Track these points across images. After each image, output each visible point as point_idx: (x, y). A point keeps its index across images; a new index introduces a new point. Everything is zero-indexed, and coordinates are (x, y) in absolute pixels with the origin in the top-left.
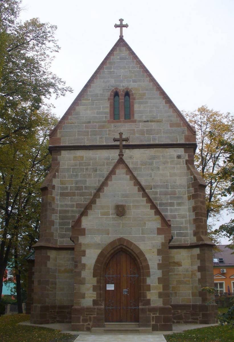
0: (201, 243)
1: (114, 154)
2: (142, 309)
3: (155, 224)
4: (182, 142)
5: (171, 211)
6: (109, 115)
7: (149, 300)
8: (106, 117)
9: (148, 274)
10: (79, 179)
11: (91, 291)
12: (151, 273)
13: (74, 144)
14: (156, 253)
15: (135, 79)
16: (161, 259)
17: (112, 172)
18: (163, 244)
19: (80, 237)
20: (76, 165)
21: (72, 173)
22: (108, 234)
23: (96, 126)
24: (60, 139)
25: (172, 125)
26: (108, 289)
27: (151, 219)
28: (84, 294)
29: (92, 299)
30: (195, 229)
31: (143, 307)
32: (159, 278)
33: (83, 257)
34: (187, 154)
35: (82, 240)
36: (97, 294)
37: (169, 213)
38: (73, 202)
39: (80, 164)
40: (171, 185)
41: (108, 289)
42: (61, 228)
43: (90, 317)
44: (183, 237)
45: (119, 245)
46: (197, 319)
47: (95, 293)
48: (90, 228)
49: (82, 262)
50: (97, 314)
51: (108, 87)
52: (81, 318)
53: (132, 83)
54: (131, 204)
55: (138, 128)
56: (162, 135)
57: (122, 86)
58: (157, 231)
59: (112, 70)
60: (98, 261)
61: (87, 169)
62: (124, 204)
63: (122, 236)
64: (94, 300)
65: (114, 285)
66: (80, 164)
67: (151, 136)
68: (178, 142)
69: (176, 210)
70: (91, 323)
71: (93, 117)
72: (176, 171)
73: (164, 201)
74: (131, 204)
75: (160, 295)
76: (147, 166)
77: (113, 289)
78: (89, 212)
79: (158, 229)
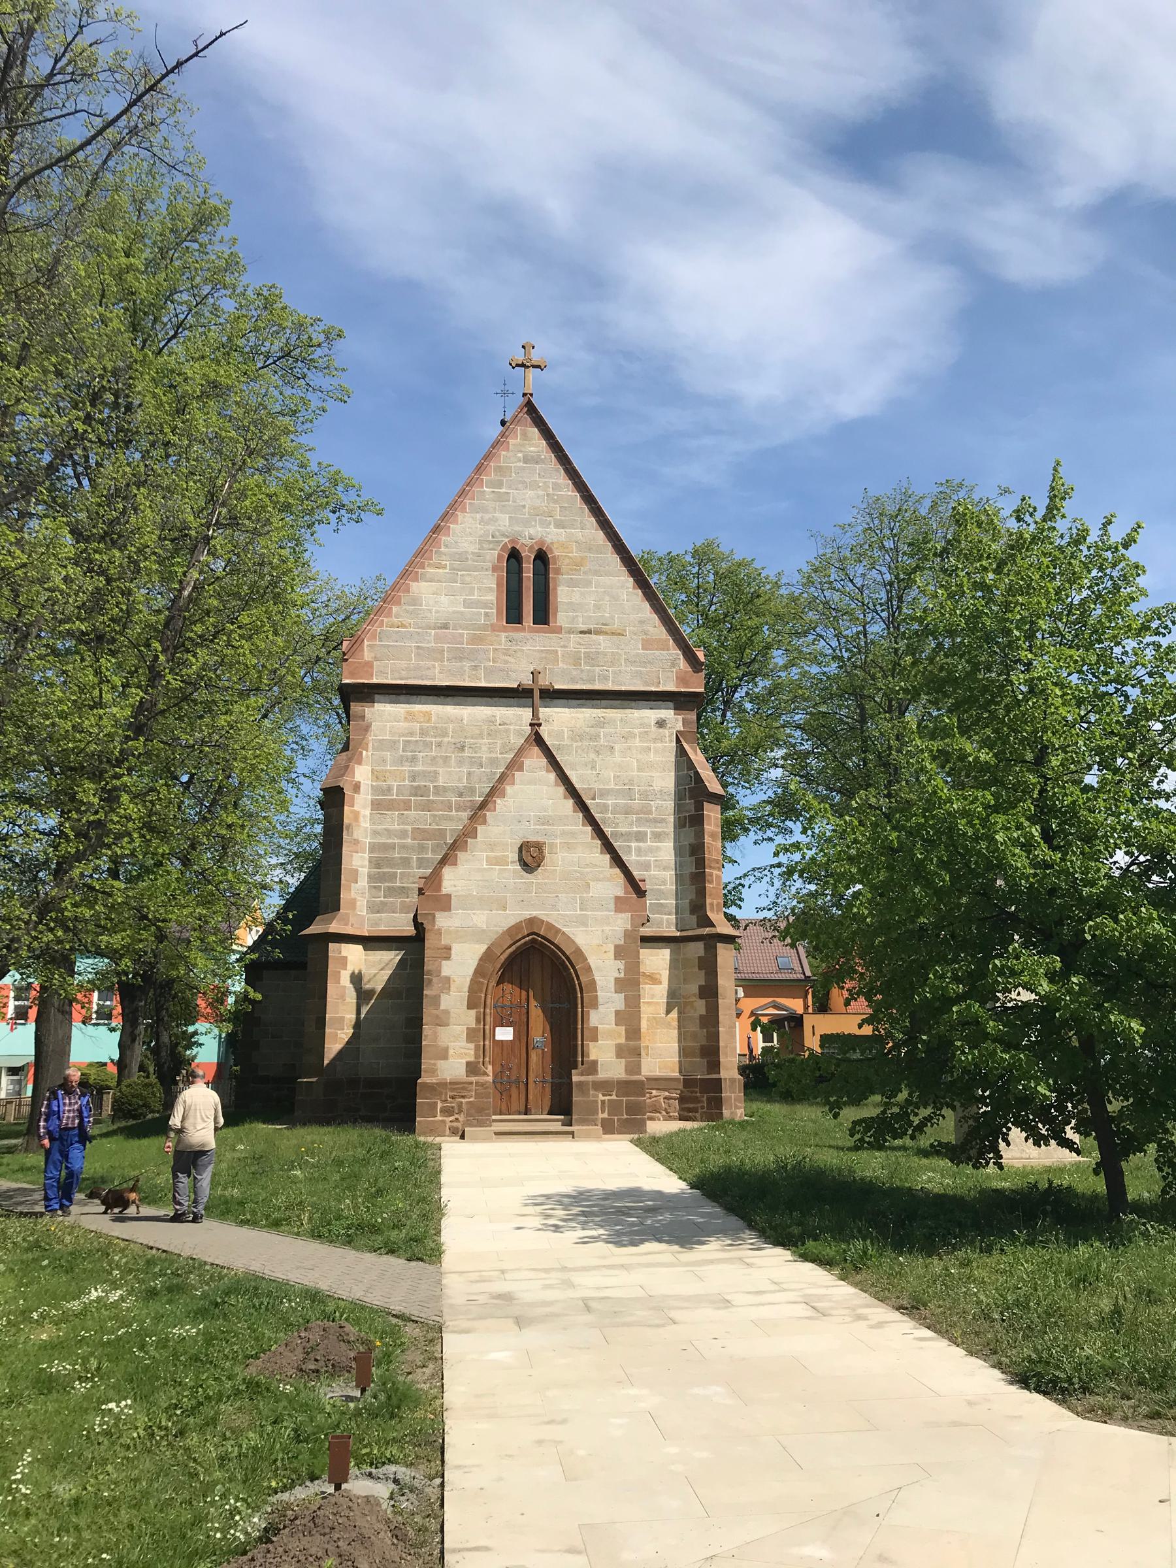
0: (707, 930)
1: (518, 717)
2: (580, 1084)
3: (613, 885)
4: (671, 687)
5: (639, 851)
6: (495, 611)
7: (595, 1063)
8: (486, 614)
9: (595, 1005)
10: (419, 768)
11: (462, 1042)
12: (600, 1000)
13: (407, 679)
14: (611, 954)
15: (561, 520)
16: (622, 967)
17: (515, 765)
18: (627, 934)
19: (438, 915)
20: (412, 734)
21: (401, 753)
22: (505, 908)
23: (462, 635)
24: (369, 665)
25: (646, 645)
26: (498, 1038)
27: (601, 876)
28: (446, 1049)
29: (464, 1061)
30: (693, 896)
31: (582, 1078)
32: (617, 1013)
33: (444, 962)
34: (680, 718)
35: (443, 921)
36: (477, 1048)
37: (634, 858)
38: (406, 824)
39: (423, 732)
40: (639, 791)
41: (498, 1038)
42: (375, 887)
43: (460, 1105)
44: (665, 914)
45: (528, 935)
46: (695, 1110)
47: (472, 1046)
48: (461, 893)
49: (443, 974)
50: (477, 1095)
51: (493, 537)
52: (440, 1105)
53: (552, 529)
54: (558, 841)
55: (564, 646)
56: (623, 668)
57: (530, 535)
58: (616, 904)
59: (503, 490)
60: (479, 972)
61: (439, 745)
62: (540, 839)
63: (535, 913)
64: (468, 1064)
65: (511, 1029)
66: (423, 732)
67: (597, 669)
68: (661, 688)
69: (651, 850)
70: (462, 1118)
71: (454, 612)
72: (652, 757)
73: (623, 829)
74: (558, 841)
75: (620, 1052)
76: (586, 743)
77: (510, 1037)
78: (461, 856)
79: (617, 898)
